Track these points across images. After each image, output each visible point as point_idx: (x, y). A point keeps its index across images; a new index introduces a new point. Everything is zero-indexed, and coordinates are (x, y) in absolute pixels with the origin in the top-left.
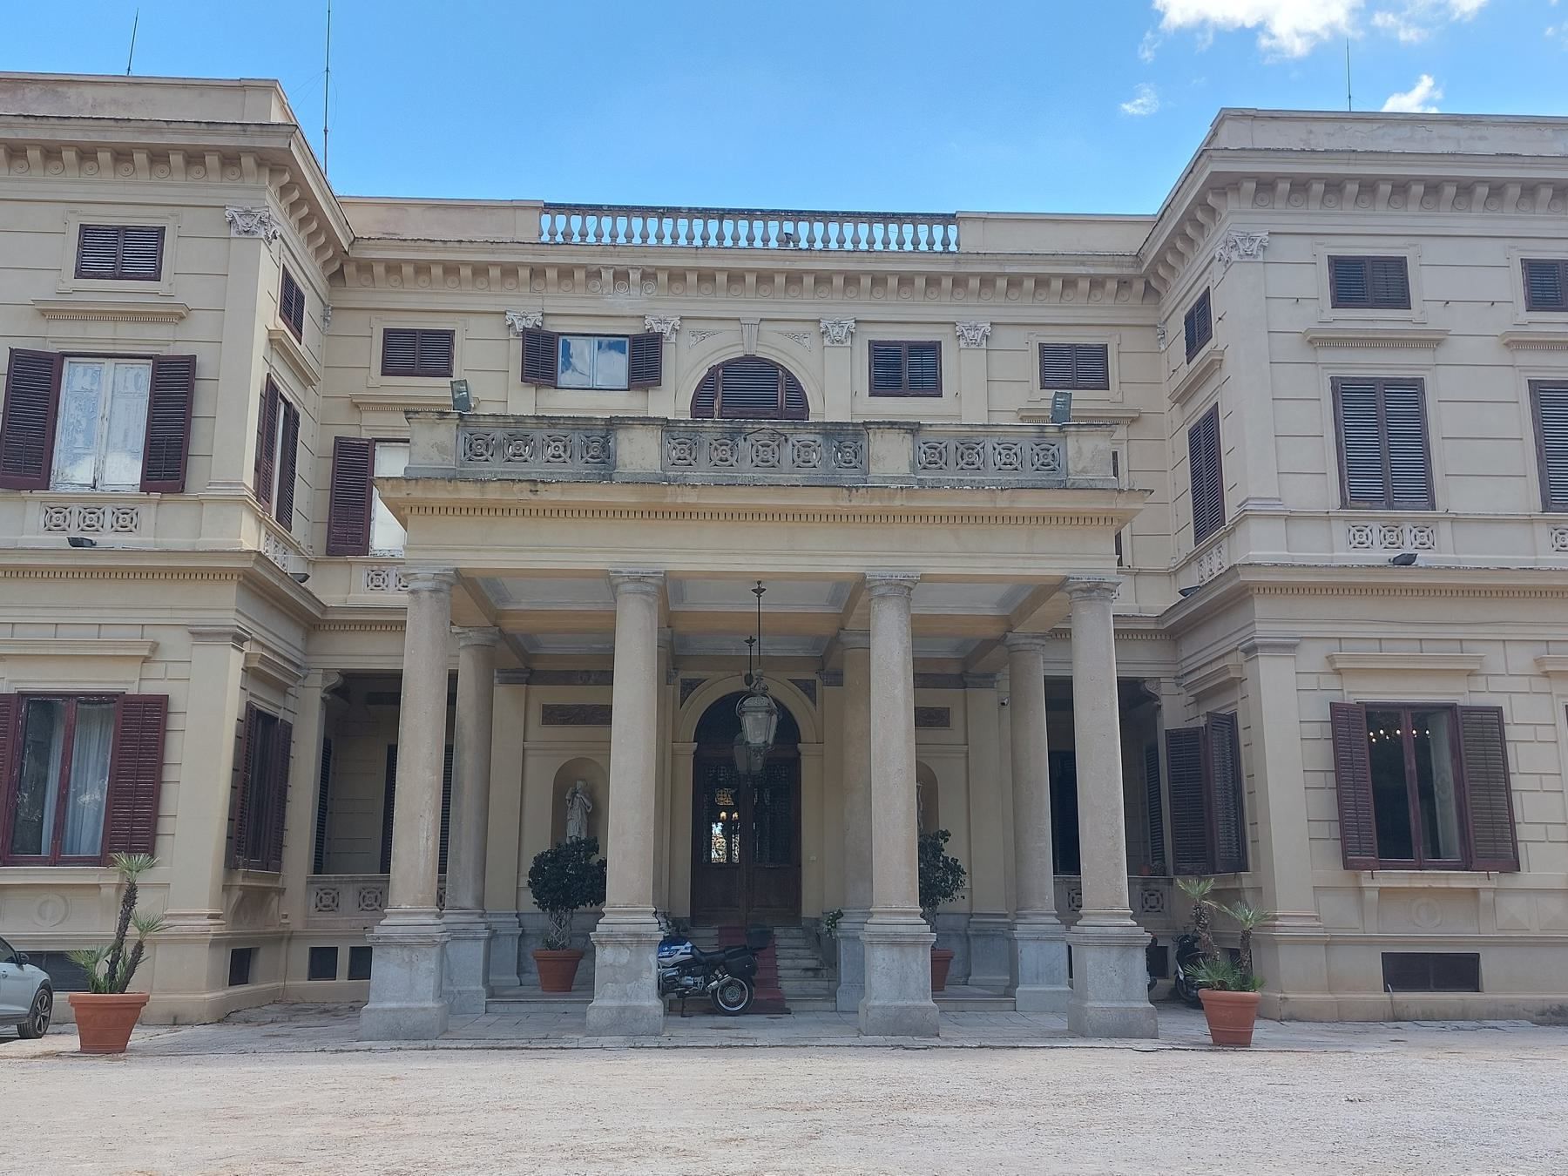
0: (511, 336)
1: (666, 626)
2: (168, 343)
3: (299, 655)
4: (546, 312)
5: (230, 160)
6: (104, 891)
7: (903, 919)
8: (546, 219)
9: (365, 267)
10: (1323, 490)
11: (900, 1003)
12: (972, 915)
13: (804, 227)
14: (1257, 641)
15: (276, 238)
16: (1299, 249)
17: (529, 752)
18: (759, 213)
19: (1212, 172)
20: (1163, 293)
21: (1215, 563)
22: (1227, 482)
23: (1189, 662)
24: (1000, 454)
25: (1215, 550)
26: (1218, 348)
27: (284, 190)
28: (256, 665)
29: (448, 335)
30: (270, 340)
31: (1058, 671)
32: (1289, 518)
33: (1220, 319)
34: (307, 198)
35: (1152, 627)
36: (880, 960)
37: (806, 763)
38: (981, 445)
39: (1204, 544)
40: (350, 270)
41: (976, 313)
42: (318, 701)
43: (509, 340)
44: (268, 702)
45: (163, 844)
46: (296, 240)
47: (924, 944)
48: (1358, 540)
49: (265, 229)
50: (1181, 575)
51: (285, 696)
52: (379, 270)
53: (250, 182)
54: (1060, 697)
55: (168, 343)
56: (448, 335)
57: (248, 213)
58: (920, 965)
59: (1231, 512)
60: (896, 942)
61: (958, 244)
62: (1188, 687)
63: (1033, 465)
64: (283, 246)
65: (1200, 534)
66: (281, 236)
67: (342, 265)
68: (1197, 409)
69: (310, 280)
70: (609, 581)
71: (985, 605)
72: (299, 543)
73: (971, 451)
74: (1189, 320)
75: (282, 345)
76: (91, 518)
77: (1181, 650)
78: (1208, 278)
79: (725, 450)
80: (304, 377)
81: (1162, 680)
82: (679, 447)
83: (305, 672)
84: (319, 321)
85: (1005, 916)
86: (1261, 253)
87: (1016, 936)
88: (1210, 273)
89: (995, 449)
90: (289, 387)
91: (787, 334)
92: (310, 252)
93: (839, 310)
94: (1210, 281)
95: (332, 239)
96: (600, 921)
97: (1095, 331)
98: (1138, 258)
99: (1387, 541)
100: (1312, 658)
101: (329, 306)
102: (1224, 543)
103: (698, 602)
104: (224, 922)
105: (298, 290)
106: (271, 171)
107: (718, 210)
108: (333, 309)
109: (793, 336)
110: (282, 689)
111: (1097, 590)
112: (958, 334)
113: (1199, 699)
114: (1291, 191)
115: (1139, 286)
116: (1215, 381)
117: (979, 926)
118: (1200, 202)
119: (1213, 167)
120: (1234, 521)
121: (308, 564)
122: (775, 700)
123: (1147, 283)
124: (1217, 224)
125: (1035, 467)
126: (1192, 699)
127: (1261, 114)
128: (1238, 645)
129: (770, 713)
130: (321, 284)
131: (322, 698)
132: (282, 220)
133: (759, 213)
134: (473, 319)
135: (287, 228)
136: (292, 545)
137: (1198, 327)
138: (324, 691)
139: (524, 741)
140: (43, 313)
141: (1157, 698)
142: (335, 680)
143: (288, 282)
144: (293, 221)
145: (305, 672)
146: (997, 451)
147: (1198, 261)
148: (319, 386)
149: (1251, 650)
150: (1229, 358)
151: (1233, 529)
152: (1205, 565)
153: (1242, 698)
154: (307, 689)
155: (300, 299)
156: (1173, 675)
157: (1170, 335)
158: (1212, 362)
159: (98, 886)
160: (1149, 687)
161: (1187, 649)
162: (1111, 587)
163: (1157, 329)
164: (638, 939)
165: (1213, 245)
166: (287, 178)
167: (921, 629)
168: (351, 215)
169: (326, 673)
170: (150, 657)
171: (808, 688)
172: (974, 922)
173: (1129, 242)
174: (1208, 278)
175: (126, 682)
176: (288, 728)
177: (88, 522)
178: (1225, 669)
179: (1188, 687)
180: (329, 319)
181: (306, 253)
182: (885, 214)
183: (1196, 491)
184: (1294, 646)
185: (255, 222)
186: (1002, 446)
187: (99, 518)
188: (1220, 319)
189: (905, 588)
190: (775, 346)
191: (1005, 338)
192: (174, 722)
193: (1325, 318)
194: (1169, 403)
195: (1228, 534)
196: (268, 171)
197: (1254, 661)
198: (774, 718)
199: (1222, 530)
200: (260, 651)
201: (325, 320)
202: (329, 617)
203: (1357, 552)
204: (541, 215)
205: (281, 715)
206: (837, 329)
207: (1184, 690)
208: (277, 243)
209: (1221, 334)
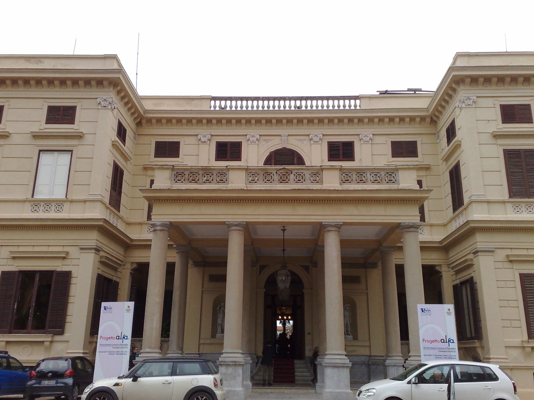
0: (200, 143)
1: (251, 244)
2: (76, 146)
3: (122, 257)
4: (212, 134)
5: (100, 82)
6: (45, 343)
7: (338, 357)
8: (213, 102)
9: (149, 121)
10: (503, 193)
11: (338, 391)
12: (370, 356)
13: (304, 102)
14: (478, 249)
15: (115, 109)
16: (489, 102)
17: (204, 292)
18: (287, 98)
19: (453, 75)
20: (437, 121)
21: (461, 221)
22: (464, 189)
23: (452, 258)
24: (373, 177)
25: (460, 215)
26: (459, 140)
27: (119, 92)
28: (104, 260)
29: (178, 143)
30: (113, 144)
31: (399, 262)
32: (488, 202)
33: (459, 129)
34: (126, 95)
35: (438, 245)
36: (329, 372)
37: (306, 297)
38: (366, 174)
39: (457, 212)
40: (144, 121)
41: (366, 131)
42: (129, 274)
43: (199, 144)
44: (108, 273)
45: (68, 326)
46: (123, 110)
47: (347, 367)
48: (517, 210)
49: (111, 105)
50: (448, 226)
51: (116, 272)
52: (154, 121)
53: (106, 90)
54: (400, 270)
55: (76, 146)
56: (178, 143)
57: (105, 100)
58: (345, 374)
59: (466, 201)
60: (335, 366)
61: (360, 106)
62: (452, 268)
63: (386, 181)
64: (118, 112)
65: (455, 210)
66: (117, 108)
67: (141, 120)
68: (452, 163)
69: (129, 124)
70: (228, 226)
71: (370, 234)
72: (122, 217)
73: (361, 176)
74: (448, 131)
75: (117, 146)
76: (47, 208)
77: (449, 254)
78: (454, 115)
79: (269, 177)
80: (126, 158)
81: (442, 266)
82: (252, 176)
83: (124, 263)
84: (132, 139)
85: (383, 356)
86: (474, 105)
87: (386, 364)
88: (455, 113)
89: (371, 175)
90: (121, 163)
91: (298, 140)
92: (129, 114)
93: (316, 132)
94: (455, 115)
95: (137, 110)
96: (221, 356)
97: (412, 136)
98: (427, 109)
99: (528, 210)
100: (501, 255)
101: (136, 134)
102: (464, 212)
103: (263, 234)
104: (89, 355)
105: (124, 128)
106: (114, 86)
107: (273, 97)
108: (138, 135)
109: (300, 140)
110: (115, 269)
111: (413, 228)
112: (360, 138)
113: (457, 272)
114: (484, 82)
115: (428, 120)
116: (458, 152)
117: (373, 361)
118: (450, 87)
119: (453, 73)
120: (468, 204)
121: (127, 224)
122: (289, 271)
123: (432, 118)
124: (457, 94)
125: (386, 181)
126: (454, 273)
127: (471, 54)
128: (471, 251)
129: (287, 276)
130: (133, 126)
131: (130, 273)
132: (118, 103)
133: (287, 98)
134: (186, 138)
135: (120, 105)
136: (120, 218)
137: (451, 132)
138: (131, 270)
139: (202, 288)
140: (34, 136)
141: (441, 273)
142: (135, 266)
143: (120, 125)
144: (122, 103)
145: (124, 263)
146: (372, 176)
147: (449, 109)
148: (131, 161)
149: (476, 253)
150: (463, 147)
151: (467, 207)
152: (457, 221)
153: (473, 272)
154: (125, 270)
155: (125, 131)
156: (446, 264)
157: (441, 137)
158: (457, 145)
159: (43, 342)
160: (438, 268)
161: (452, 253)
162: (417, 226)
163: (436, 134)
164: (236, 364)
165: (456, 102)
166: (119, 88)
167: (344, 244)
168: (144, 103)
169: (132, 263)
170: (66, 257)
171: (306, 268)
172: (372, 359)
173: (422, 104)
174: (454, 115)
175: (57, 266)
176: (117, 283)
177: (46, 209)
178: (466, 261)
179: (452, 268)
180: (136, 138)
181: (128, 115)
182: (333, 97)
183: (453, 193)
184: (493, 251)
185: (108, 103)
186: (374, 174)
187: (50, 207)
188: (459, 129)
189: (338, 227)
190: (294, 144)
191: (378, 139)
192: (73, 281)
193: (499, 127)
194: (441, 161)
195: (465, 209)
196: (112, 86)
197: (477, 257)
198: (290, 278)
199: (463, 207)
200: (106, 255)
201: (135, 138)
202: (133, 243)
203: (516, 215)
204: (211, 101)
205: (114, 279)
206: (316, 138)
207: (451, 270)
208: (116, 111)
209: (460, 135)
